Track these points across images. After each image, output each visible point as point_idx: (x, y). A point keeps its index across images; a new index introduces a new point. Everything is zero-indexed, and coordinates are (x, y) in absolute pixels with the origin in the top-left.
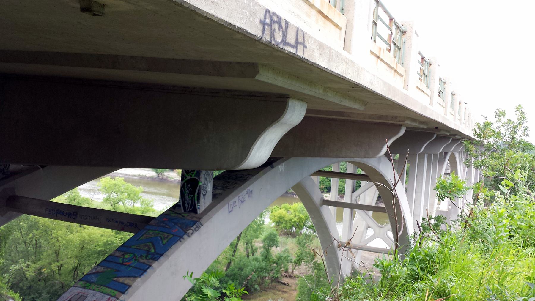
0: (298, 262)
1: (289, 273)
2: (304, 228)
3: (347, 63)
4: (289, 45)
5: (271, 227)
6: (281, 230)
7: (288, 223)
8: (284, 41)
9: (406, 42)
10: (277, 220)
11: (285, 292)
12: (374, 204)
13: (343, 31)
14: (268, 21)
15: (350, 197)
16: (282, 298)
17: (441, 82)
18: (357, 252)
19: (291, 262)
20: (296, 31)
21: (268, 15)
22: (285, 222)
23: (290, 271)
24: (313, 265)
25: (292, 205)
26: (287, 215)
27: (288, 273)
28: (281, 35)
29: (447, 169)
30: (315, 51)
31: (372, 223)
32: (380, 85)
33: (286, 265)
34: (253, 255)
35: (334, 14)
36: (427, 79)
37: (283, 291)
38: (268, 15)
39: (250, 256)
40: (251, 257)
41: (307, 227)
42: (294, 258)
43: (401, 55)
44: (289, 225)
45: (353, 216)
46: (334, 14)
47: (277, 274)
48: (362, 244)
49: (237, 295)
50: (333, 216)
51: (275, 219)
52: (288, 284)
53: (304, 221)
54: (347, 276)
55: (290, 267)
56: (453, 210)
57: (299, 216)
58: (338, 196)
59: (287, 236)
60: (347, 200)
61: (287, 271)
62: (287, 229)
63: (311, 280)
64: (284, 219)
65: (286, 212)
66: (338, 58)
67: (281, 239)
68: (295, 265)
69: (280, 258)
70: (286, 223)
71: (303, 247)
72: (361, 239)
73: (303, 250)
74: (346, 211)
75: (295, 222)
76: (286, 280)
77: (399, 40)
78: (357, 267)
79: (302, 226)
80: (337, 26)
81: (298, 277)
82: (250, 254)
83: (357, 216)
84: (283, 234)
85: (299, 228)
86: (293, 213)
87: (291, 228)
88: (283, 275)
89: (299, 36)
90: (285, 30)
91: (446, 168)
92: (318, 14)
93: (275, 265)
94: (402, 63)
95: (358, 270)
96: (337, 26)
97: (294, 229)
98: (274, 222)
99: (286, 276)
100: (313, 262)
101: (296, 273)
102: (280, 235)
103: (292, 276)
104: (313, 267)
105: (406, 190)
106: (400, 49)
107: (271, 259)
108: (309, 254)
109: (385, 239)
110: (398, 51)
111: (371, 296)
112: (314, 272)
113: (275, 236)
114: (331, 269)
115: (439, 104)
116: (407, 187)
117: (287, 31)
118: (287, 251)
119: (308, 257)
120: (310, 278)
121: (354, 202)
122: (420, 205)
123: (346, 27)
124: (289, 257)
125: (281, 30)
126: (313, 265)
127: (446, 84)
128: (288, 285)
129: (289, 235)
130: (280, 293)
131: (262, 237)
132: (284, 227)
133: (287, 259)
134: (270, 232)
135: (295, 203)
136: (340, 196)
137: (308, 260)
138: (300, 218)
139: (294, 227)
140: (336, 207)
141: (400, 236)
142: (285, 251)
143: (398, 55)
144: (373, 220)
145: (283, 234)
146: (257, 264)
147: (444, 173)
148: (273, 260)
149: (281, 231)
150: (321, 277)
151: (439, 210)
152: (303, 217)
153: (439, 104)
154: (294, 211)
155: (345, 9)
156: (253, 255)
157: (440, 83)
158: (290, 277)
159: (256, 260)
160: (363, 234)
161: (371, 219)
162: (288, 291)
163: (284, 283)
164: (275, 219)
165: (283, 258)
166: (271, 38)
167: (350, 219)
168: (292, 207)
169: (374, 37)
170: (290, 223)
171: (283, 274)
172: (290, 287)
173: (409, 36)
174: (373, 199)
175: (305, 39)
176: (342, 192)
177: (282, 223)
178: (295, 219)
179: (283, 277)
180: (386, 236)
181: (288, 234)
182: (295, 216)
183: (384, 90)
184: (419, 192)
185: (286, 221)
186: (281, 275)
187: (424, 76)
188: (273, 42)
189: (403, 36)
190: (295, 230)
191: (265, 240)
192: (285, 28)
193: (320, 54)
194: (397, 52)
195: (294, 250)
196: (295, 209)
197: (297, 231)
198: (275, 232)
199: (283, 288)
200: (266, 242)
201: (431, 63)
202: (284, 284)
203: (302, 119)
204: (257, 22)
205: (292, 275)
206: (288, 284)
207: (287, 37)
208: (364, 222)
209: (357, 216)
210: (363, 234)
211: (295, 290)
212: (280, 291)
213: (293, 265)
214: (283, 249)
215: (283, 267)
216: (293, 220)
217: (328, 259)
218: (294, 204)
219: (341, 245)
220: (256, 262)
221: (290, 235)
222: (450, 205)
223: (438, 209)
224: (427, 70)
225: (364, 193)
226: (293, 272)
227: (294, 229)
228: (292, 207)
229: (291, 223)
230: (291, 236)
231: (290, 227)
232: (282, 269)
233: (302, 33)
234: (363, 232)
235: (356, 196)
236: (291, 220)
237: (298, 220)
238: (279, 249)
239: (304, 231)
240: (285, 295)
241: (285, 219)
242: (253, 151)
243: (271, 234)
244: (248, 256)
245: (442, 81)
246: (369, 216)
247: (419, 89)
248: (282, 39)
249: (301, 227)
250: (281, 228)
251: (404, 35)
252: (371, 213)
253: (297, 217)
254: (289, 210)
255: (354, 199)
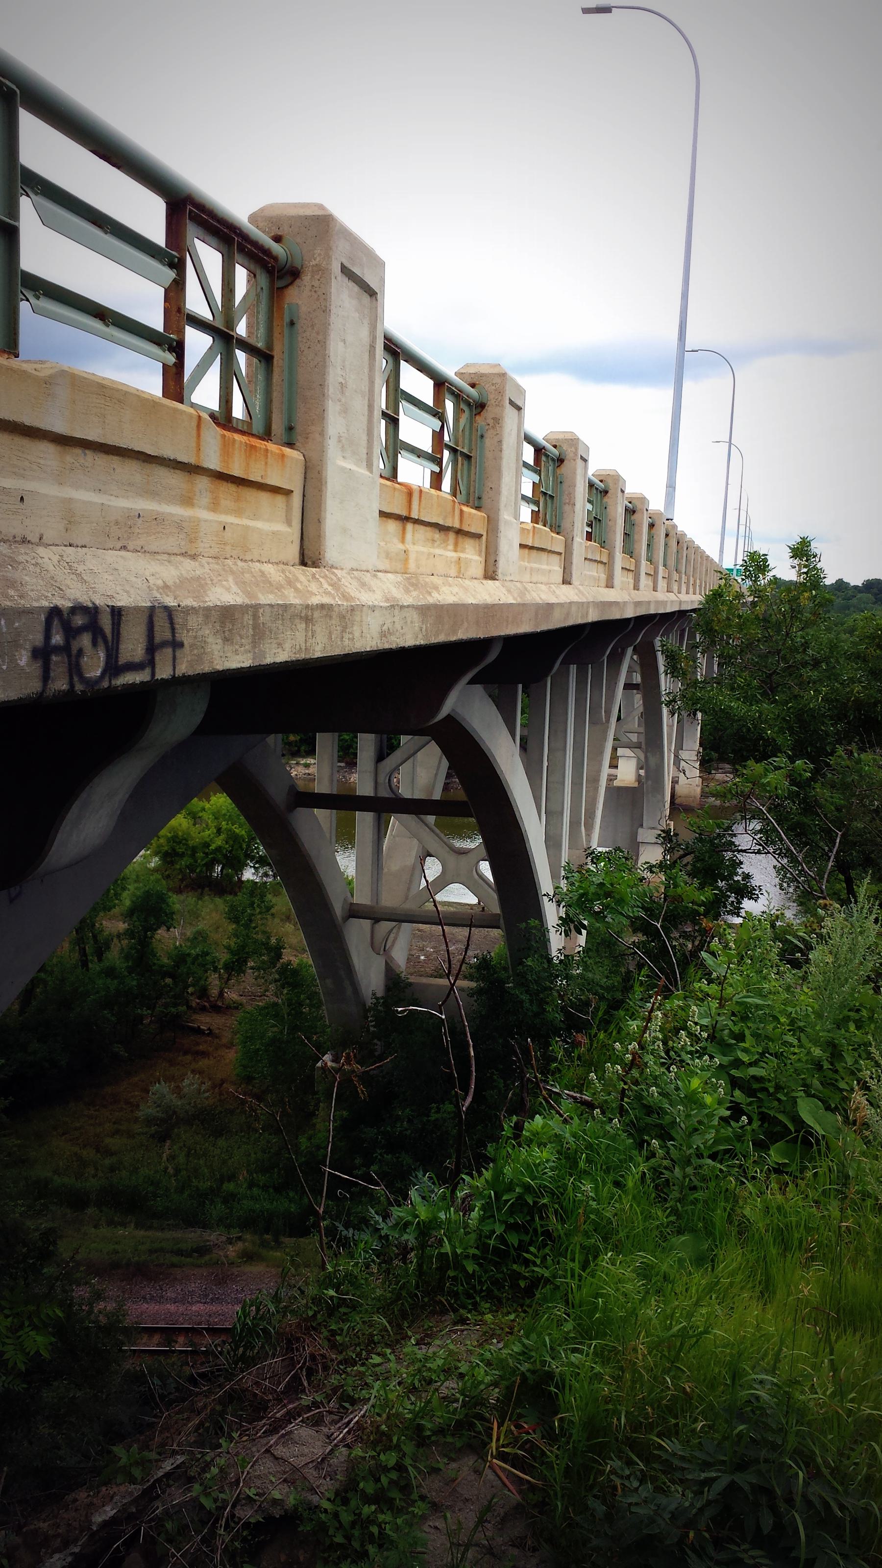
0: (236, 967)
1: (212, 999)
2: (247, 865)
3: (308, 620)
4: (132, 667)
5: (149, 869)
6: (180, 877)
7: (200, 855)
8: (113, 667)
9: (486, 435)
10: (166, 848)
11: (204, 1054)
12: (437, 796)
13: (296, 500)
14: (57, 639)
15: (373, 775)
16: (193, 1071)
17: (595, 491)
18: (399, 928)
19: (216, 970)
20: (146, 621)
21: (56, 622)
22: (189, 852)
23: (214, 992)
24: (277, 976)
25: (209, 801)
26: (194, 831)
27: (208, 998)
28: (102, 655)
29: (630, 671)
30: (210, 640)
31: (433, 844)
32: (412, 622)
33: (201, 978)
34: (100, 960)
35: (266, 463)
36: (552, 503)
37: (197, 1053)
38: (56, 622)
39: (92, 961)
40: (95, 966)
41: (257, 862)
42: (224, 957)
43: (473, 472)
44: (202, 860)
45: (383, 827)
46: (266, 463)
47: (175, 1005)
48: (410, 906)
49: (35, 1320)
50: (328, 835)
51: (160, 846)
52: (209, 1029)
53: (244, 846)
54: (374, 994)
55: (214, 981)
56: (650, 782)
57: (230, 830)
58: (339, 762)
59: (200, 891)
60: (364, 786)
61: (203, 993)
62: (198, 871)
63: (276, 1016)
64: (187, 845)
65: (191, 822)
66: (280, 622)
67: (177, 902)
68: (226, 975)
69: (181, 958)
70: (193, 855)
71: (247, 926)
72: (409, 889)
73: (247, 935)
74: (364, 820)
75: (219, 849)
76: (204, 1021)
77: (467, 433)
78: (400, 967)
79: (242, 857)
80: (275, 490)
81: (236, 1008)
82: (90, 958)
83: (393, 826)
84: (187, 886)
85: (233, 868)
86: (213, 825)
87: (210, 866)
88: (194, 1005)
89: (156, 628)
90: (113, 636)
91: (629, 667)
92: (218, 481)
93: (168, 981)
94: (477, 496)
95: (403, 975)
96: (275, 490)
97: (218, 869)
98: (156, 854)
99: (203, 1009)
100: (278, 965)
101: (232, 995)
102: (179, 891)
103: (220, 1007)
104: (279, 981)
105: (524, 747)
106: (468, 457)
107: (154, 964)
108: (266, 945)
109: (473, 883)
110: (466, 463)
111: (373, 1406)
112: (282, 993)
113: (162, 898)
114: (329, 982)
115: (590, 560)
116: (526, 733)
117: (119, 633)
118: (200, 937)
119: (264, 955)
120: (272, 1011)
121: (384, 793)
122: (563, 783)
123: (305, 481)
124: (207, 954)
125: (100, 640)
126: (277, 976)
127: (609, 495)
128: (208, 1035)
129: (203, 889)
130: (189, 1057)
131: (127, 900)
132: (187, 867)
133: (204, 962)
134: (147, 889)
135: (215, 794)
136: (347, 763)
137: (263, 962)
138: (234, 838)
139: (219, 863)
140: (334, 811)
141: (467, 1109)
142: (196, 938)
143: (465, 472)
144: (437, 835)
145: (187, 886)
146: (113, 984)
147: (625, 684)
148: (163, 966)
149: (182, 880)
150: (301, 1005)
151: (616, 783)
152: (243, 832)
153: (590, 560)
154: (216, 818)
155: (299, 428)
156: (100, 960)
157: (593, 499)
158: (216, 1009)
159: (110, 972)
160: (412, 875)
161: (433, 831)
162: (211, 1049)
163: (199, 1027)
164: (160, 846)
165: (189, 960)
166: (71, 678)
167: (376, 837)
168: (207, 806)
169: (391, 458)
170: (204, 853)
171: (195, 1002)
172: (217, 1037)
173: (493, 419)
174: (436, 774)
175: (177, 626)
176: (352, 750)
177: (182, 855)
178: (219, 842)
179: (194, 1012)
180: (476, 876)
181: (201, 886)
182: (219, 831)
183: (424, 630)
184: (558, 750)
185: (194, 850)
186: (189, 1007)
187: (545, 499)
188: (79, 687)
189: (477, 417)
190: (221, 870)
191: (130, 914)
192: (113, 628)
193: (226, 640)
194: (462, 464)
195: (221, 929)
196: (218, 812)
197: (227, 875)
198: (162, 886)
199: (198, 1044)
200: (135, 918)
201: (563, 457)
202: (198, 1031)
203: (199, 721)
204: (24, 659)
205: (219, 1003)
206: (209, 1029)
207: (120, 651)
208: (415, 841)
209: (393, 826)
210: (412, 875)
211: (230, 1046)
212: (186, 1053)
213: (220, 977)
214: (189, 933)
215: (193, 986)
216: (213, 847)
217: (319, 953)
218: (214, 799)
219: (354, 912)
220: (109, 981)
221: (207, 889)
222: (642, 768)
223: (611, 778)
224: (553, 476)
225: (411, 760)
226: (221, 994)
227: (218, 869)
228: (207, 806)
229: (207, 854)
230: (210, 890)
231: (206, 865)
232: (190, 990)
233: (166, 614)
234: (414, 868)
235: (388, 770)
236: (207, 845)
237: (227, 843)
238: (176, 932)
239: (248, 874)
240: (203, 1063)
241: (191, 843)
242: (59, 836)
243: (148, 895)
244: (85, 964)
245: (597, 489)
246: (426, 825)
247: (532, 548)
248: (107, 663)
249: (239, 861)
250: (180, 869)
251: (479, 413)
252: (431, 819)
253: (223, 836)
254: (200, 814)
255: (382, 778)
